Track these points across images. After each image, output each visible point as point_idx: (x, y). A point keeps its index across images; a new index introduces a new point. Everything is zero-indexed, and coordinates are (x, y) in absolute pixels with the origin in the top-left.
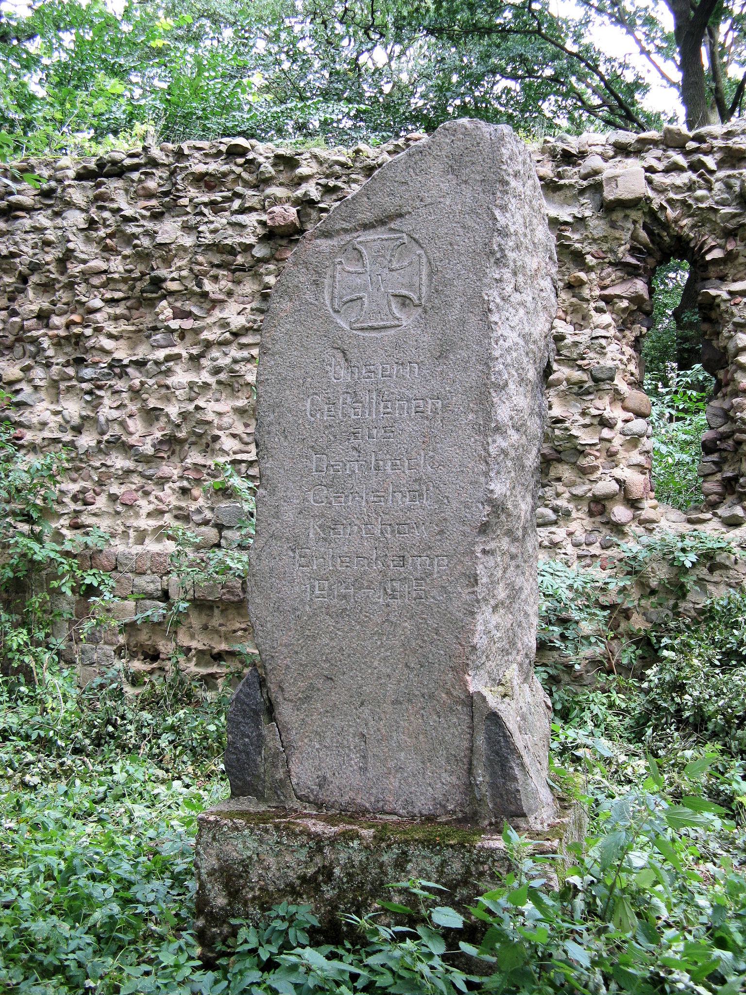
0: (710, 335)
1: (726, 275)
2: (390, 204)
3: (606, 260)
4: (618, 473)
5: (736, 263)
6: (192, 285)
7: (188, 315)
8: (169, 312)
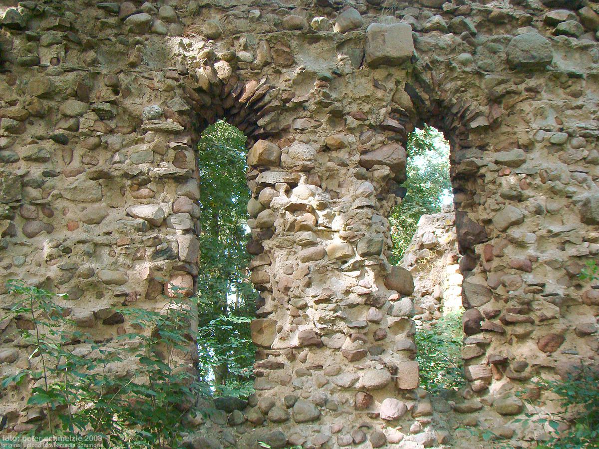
0: (464, 207)
1: (487, 144)
3: (367, 122)
5: (498, 131)
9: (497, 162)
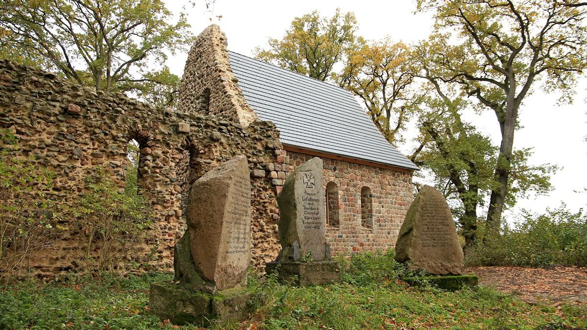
2: (310, 169)
4: (174, 208)
6: (28, 123)
7: (23, 134)
8: (15, 131)
9: (205, 162)
